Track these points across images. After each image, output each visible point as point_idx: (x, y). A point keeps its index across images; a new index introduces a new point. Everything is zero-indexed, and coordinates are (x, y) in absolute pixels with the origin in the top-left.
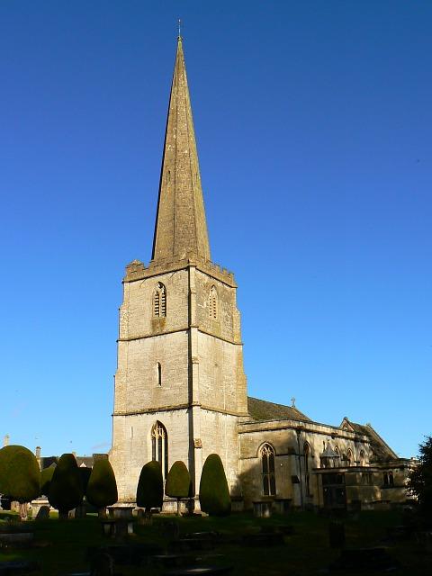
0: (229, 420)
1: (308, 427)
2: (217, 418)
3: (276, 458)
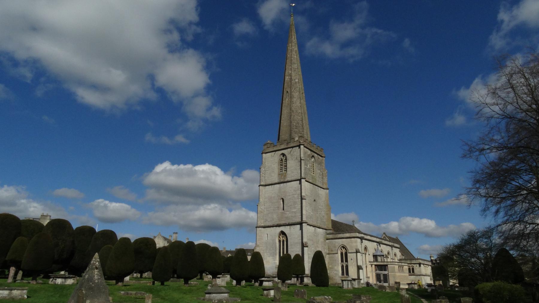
0: (350, 251)
1: (366, 237)
2: (315, 230)
3: (349, 255)
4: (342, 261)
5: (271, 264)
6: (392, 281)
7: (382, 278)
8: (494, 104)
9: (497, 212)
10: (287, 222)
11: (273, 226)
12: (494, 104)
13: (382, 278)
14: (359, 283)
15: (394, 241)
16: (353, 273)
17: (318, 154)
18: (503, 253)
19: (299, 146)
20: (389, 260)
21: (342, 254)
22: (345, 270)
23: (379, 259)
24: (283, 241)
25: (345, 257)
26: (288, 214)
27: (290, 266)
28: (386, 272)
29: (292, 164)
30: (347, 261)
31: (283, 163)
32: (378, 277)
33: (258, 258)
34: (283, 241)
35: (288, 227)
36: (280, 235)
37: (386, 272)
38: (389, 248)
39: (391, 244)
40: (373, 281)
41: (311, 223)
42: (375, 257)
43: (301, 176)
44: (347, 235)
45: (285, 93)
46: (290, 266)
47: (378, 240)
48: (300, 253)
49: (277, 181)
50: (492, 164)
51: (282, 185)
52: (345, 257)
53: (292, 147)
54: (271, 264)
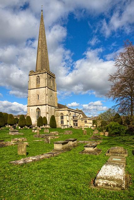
1: (70, 110)
4: (61, 119)
5: (34, 121)
6: (79, 126)
7: (75, 125)
8: (121, 60)
9: (117, 101)
10: (40, 104)
11: (36, 68)
12: (121, 60)
13: (75, 125)
14: (67, 127)
15: (80, 112)
16: (65, 123)
17: (53, 77)
18: (117, 114)
19: (45, 87)
20: (78, 118)
21: (61, 116)
22: (62, 122)
23: (75, 118)
24: (38, 112)
25: (62, 118)
26: (41, 101)
27: (41, 121)
28: (76, 123)
29: (42, 80)
30: (63, 119)
31: (38, 81)
32: (74, 124)
33: (29, 118)
34: (38, 112)
35: (41, 106)
36: (37, 109)
37: (76, 123)
38: (78, 114)
39: (79, 112)
40: (72, 125)
41: (49, 105)
42: (73, 117)
43: (46, 103)
44: (64, 109)
45: (39, 49)
46: (41, 121)
47: (75, 111)
48: (45, 116)
49: (36, 88)
50: (118, 83)
51: (38, 89)
52: (62, 118)
53: (42, 73)
54: (34, 121)
